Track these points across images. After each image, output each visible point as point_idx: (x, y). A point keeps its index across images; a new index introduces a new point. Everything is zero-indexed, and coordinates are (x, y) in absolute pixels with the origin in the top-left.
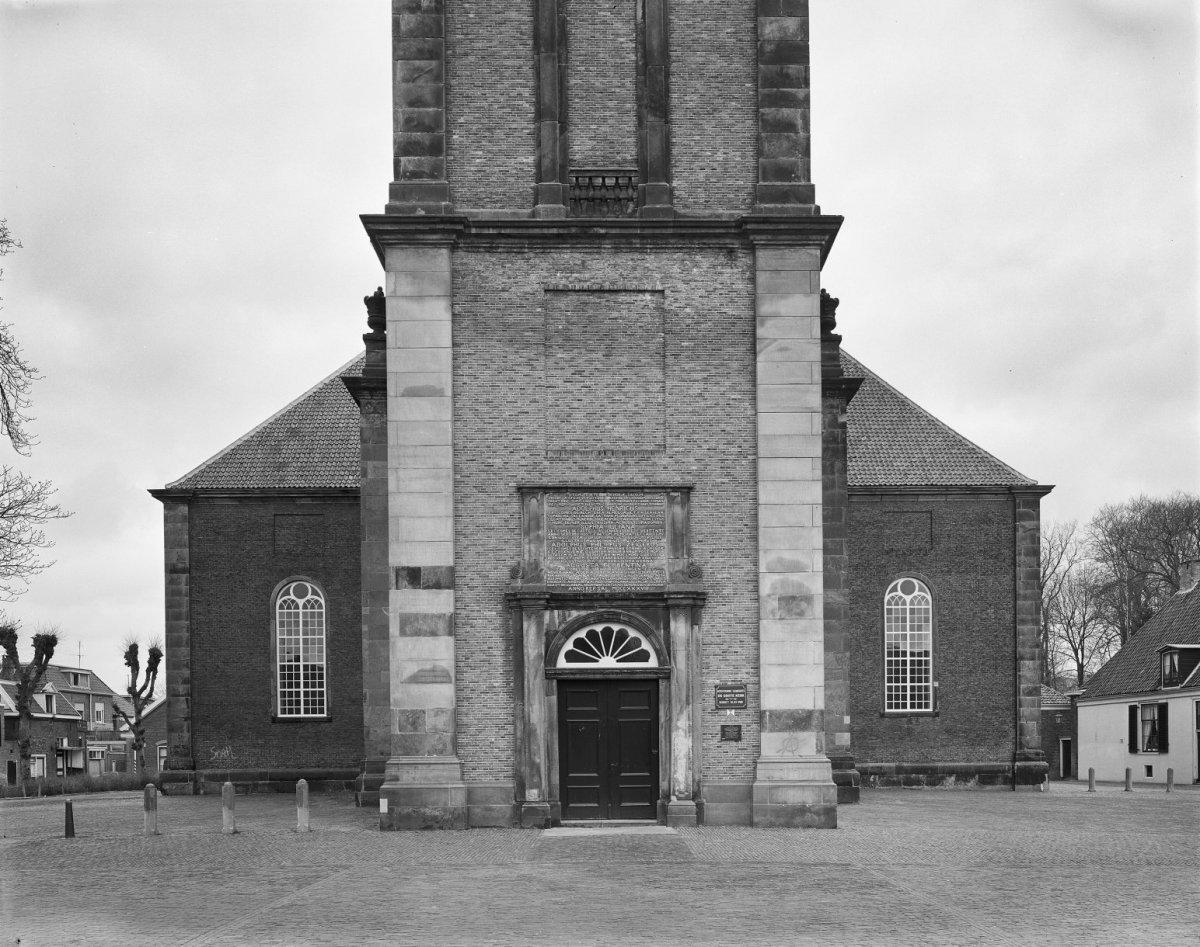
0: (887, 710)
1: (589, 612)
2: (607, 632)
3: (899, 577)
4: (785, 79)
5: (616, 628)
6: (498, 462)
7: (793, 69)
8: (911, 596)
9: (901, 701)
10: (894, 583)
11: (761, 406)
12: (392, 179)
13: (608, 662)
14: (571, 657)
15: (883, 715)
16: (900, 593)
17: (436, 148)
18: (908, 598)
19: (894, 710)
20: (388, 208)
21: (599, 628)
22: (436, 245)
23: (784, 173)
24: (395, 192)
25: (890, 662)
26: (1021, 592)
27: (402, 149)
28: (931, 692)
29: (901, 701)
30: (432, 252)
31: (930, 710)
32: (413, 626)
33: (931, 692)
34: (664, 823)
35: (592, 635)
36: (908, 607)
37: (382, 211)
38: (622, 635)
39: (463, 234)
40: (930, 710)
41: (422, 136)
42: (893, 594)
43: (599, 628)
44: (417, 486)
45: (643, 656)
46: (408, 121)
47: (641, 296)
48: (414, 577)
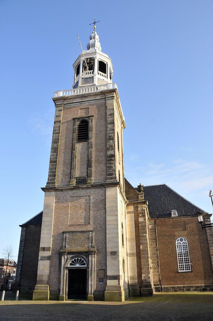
0: (179, 271)
1: (73, 256)
2: (78, 259)
3: (179, 237)
4: (111, 160)
5: (79, 258)
6: (60, 227)
7: (113, 158)
8: (182, 242)
9: (183, 269)
10: (178, 239)
11: (107, 215)
12: (47, 181)
13: (78, 265)
14: (71, 264)
15: (178, 272)
16: (179, 241)
17: (55, 176)
18: (182, 242)
19: (181, 271)
20: (46, 186)
21: (76, 259)
22: (53, 191)
23: (111, 175)
24: (48, 183)
25: (179, 259)
26: (209, 239)
27: (49, 176)
28: (190, 266)
29: (183, 269)
30: (52, 192)
31: (190, 270)
32: (43, 258)
33: (190, 266)
34: (87, 300)
35: (75, 260)
36: (182, 245)
37: (45, 187)
38: (81, 260)
39: (56, 190)
40: (190, 270)
41: (52, 175)
42: (178, 242)
43: (82, 260)
44: (46, 232)
45: (84, 264)
46: (50, 172)
47: (86, 197)
48: (44, 249)
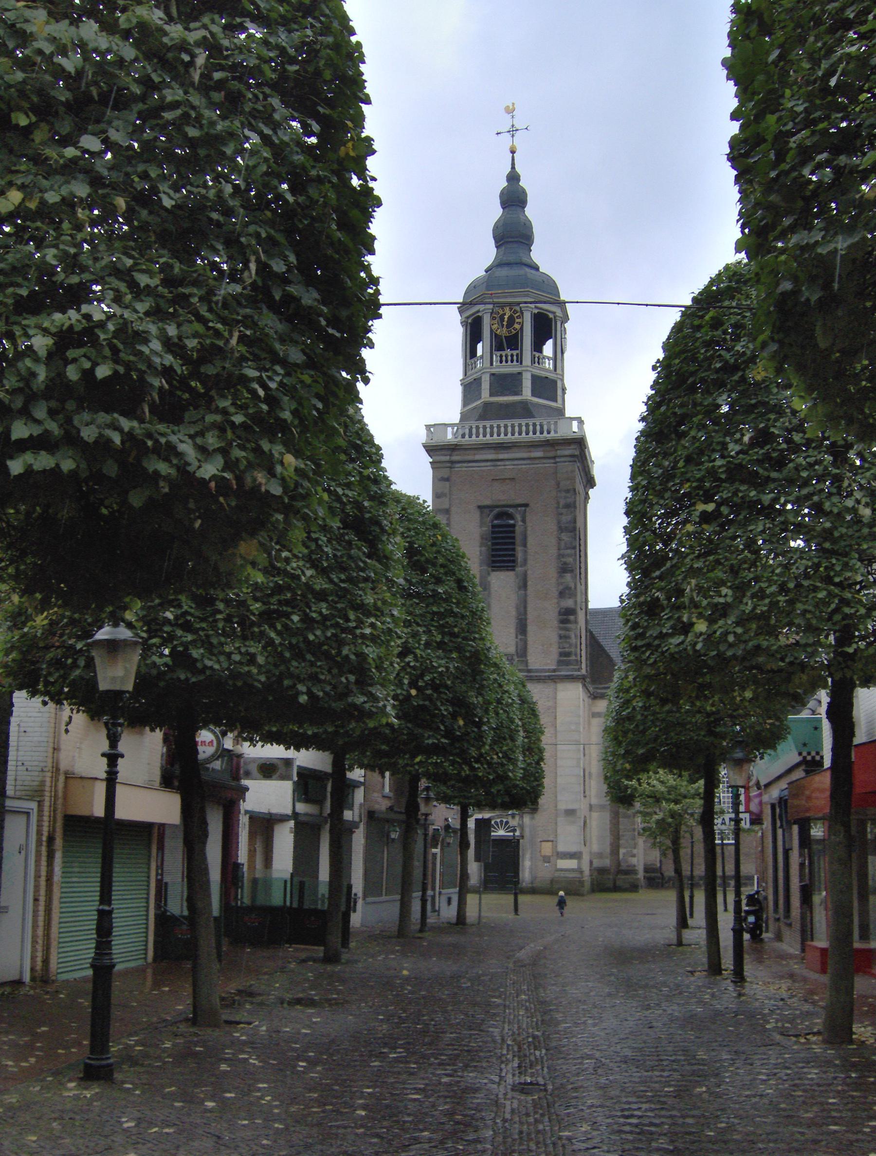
7: (572, 618)
